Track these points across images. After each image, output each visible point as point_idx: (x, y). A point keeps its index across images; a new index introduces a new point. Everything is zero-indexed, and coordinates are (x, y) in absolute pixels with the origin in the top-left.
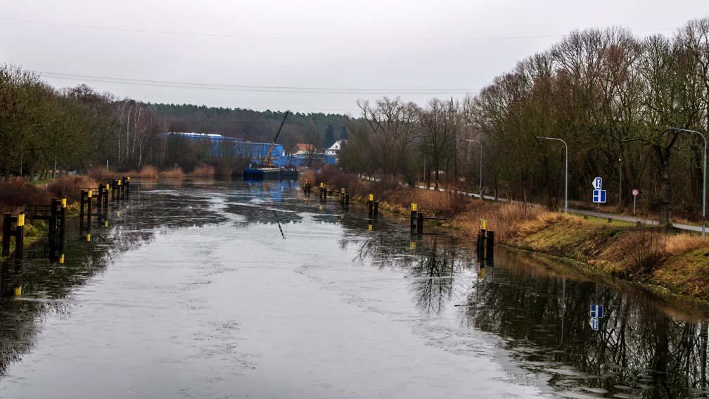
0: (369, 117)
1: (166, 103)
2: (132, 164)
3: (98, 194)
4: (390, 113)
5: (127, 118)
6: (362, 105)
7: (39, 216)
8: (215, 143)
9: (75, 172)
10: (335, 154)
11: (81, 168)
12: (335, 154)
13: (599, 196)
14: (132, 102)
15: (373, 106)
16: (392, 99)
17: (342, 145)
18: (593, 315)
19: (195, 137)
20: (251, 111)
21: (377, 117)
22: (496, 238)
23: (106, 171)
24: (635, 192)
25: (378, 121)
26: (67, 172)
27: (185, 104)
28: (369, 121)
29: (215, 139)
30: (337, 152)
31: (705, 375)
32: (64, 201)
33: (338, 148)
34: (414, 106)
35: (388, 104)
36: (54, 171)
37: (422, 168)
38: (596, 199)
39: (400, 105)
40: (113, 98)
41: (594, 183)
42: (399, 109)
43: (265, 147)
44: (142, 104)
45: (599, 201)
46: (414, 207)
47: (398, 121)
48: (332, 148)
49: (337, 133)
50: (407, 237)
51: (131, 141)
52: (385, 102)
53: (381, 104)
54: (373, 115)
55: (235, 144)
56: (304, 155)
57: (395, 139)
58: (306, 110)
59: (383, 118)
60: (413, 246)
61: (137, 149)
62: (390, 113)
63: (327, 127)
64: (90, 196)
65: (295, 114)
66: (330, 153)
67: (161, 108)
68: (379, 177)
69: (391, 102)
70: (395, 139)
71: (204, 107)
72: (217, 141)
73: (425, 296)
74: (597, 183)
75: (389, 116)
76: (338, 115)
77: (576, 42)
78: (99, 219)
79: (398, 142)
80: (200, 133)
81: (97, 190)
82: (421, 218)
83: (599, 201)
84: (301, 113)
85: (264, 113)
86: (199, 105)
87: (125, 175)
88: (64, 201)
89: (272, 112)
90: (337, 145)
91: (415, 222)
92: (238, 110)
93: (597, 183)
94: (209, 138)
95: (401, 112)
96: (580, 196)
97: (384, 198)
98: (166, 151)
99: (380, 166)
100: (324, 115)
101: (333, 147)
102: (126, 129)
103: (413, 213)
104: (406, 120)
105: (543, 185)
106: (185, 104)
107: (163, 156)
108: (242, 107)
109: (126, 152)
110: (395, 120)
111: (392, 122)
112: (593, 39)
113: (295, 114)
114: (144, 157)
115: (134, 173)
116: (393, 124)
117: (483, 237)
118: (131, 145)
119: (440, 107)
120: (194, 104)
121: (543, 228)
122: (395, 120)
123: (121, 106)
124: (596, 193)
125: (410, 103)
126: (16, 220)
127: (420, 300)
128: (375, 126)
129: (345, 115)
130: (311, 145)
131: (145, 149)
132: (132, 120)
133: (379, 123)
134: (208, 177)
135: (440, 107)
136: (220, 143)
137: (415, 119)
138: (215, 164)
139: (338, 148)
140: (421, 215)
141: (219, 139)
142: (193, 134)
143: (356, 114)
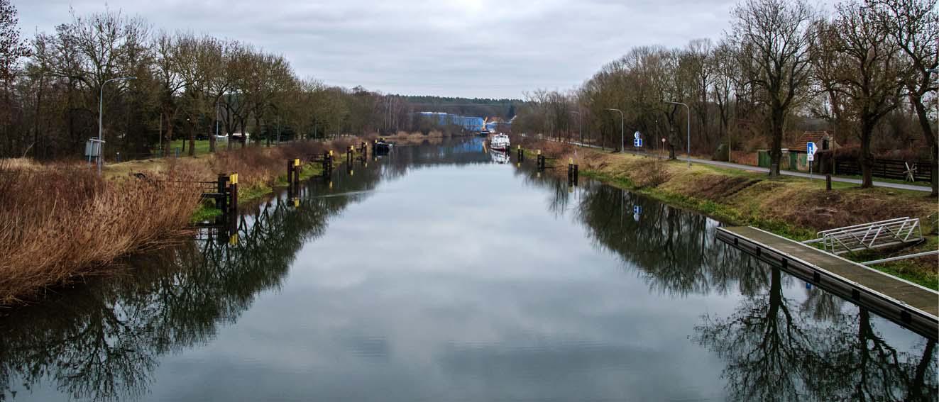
13: (638, 142)
16: (543, 89)
18: (636, 212)
19: (431, 115)
22: (579, 169)
24: (664, 140)
27: (476, 99)
29: (442, 115)
31: (190, 147)
38: (637, 144)
41: (635, 135)
42: (547, 95)
45: (638, 145)
51: (392, 117)
58: (498, 98)
61: (395, 122)
68: (540, 138)
73: (554, 204)
74: (637, 135)
77: (635, 52)
78: (362, 163)
82: (543, 159)
83: (638, 145)
84: (495, 99)
86: (436, 96)
91: (540, 161)
93: (637, 135)
94: (438, 115)
96: (629, 143)
105: (614, 138)
106: (476, 99)
107: (410, 126)
112: (645, 51)
114: (400, 126)
115: (394, 136)
117: (572, 169)
121: (622, 163)
124: (636, 141)
126: (294, 162)
127: (551, 207)
132: (392, 106)
138: (442, 130)
140: (543, 157)
141: (444, 115)
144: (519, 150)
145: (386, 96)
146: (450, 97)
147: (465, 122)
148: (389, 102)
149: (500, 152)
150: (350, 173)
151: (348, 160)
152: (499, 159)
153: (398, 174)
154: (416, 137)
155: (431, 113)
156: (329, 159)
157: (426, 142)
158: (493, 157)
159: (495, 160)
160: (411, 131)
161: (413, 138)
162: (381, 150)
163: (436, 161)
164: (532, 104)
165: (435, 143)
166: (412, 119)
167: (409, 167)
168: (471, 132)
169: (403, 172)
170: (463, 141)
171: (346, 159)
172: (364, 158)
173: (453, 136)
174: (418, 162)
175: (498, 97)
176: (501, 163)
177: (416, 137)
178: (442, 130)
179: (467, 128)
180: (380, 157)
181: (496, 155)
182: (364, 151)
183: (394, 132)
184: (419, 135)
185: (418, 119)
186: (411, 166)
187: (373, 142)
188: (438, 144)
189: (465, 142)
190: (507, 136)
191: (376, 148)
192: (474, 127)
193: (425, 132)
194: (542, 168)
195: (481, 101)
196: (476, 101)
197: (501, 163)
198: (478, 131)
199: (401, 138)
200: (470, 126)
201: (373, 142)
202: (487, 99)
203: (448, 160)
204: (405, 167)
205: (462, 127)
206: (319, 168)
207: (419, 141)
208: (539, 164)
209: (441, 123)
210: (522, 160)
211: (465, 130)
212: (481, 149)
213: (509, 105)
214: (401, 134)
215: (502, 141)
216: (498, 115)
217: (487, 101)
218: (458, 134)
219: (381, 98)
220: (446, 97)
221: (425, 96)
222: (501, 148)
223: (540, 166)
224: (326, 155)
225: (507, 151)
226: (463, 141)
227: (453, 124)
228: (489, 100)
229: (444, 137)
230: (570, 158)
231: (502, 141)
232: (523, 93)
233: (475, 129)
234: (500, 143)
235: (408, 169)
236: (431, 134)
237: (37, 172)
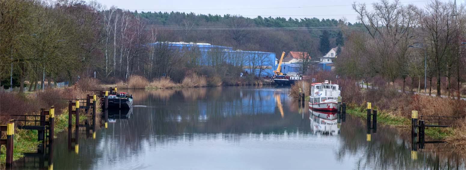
0: (366, 21)
1: (153, 12)
2: (342, 76)
3: (85, 104)
4: (388, 17)
5: (114, 27)
6: (358, 8)
7: (420, 129)
8: (204, 52)
9: (63, 83)
10: (330, 62)
11: (69, 80)
12: (330, 62)
14: (119, 11)
15: (370, 10)
17: (338, 52)
19: (185, 48)
20: (241, 18)
21: (375, 22)
23: (93, 83)
25: (376, 26)
26: (55, 84)
27: (259, 17)
28: (367, 27)
29: (204, 48)
30: (333, 59)
32: (52, 112)
33: (334, 56)
34: (414, 9)
35: (386, 7)
36: (42, 82)
37: (423, 74)
39: (399, 7)
40: (99, 7)
42: (399, 13)
43: (256, 56)
44: (128, 13)
46: (415, 114)
47: (397, 26)
48: (327, 56)
49: (332, 40)
50: (408, 145)
51: (118, 51)
52: (383, 5)
53: (378, 8)
54: (371, 20)
55: (225, 52)
56: (298, 63)
57: (394, 44)
59: (381, 23)
60: (414, 155)
61: (125, 60)
62: (388, 17)
63: (321, 34)
64: (78, 106)
65: (321, 20)
66: (325, 61)
67: (149, 17)
69: (390, 4)
70: (394, 44)
71: (192, 14)
72: (206, 50)
75: (388, 20)
76: (333, 20)
78: (88, 130)
79: (397, 47)
80: (189, 42)
81: (85, 101)
82: (422, 127)
84: (293, 18)
85: (255, 20)
86: (188, 12)
87: (112, 86)
88: (52, 112)
89: (263, 18)
90: (332, 53)
91: (417, 130)
92: (227, 17)
94: (198, 48)
95: (400, 15)
97: (384, 107)
98: (154, 62)
99: (377, 72)
100: (318, 20)
101: (329, 55)
102: (113, 38)
103: (414, 121)
104: (406, 25)
107: (150, 66)
108: (232, 14)
109: (113, 62)
110: (394, 25)
111: (391, 27)
113: (321, 20)
114: (131, 68)
115: (121, 84)
116: (395, 31)
118: (118, 56)
119: (441, 10)
120: (181, 12)
122: (394, 25)
123: (107, 16)
125: (410, 6)
128: (372, 30)
129: (340, 20)
130: (306, 53)
131: (132, 59)
132: (119, 31)
133: (377, 29)
134: (246, 85)
135: (441, 10)
136: (208, 52)
137: (416, 24)
138: (205, 73)
139: (334, 56)
142: (181, 43)
143: (352, 19)
144: (369, 111)
145: (108, 12)
146: (213, 14)
147: (247, 60)
148: (112, 21)
149: (325, 115)
150: (74, 149)
151: (70, 126)
152: (322, 128)
153: (129, 150)
154: (161, 87)
155: (184, 43)
156: (47, 123)
157: (178, 96)
158: (313, 124)
159: (315, 129)
160: (151, 77)
161: (157, 88)
162: (116, 108)
163: (192, 130)
164: (372, 30)
165: (195, 97)
166: (152, 55)
167: (148, 139)
168: (257, 78)
169: (136, 149)
170: (241, 94)
171: (67, 123)
172: (90, 123)
173: (226, 85)
174: (167, 130)
175: (298, 14)
176: (326, 134)
177: (161, 87)
178: (205, 73)
179: (249, 71)
180: (112, 121)
181: (316, 119)
182: (91, 110)
183: (122, 76)
184: (166, 82)
185: (163, 53)
186: (152, 139)
187: (101, 94)
188: (199, 98)
189: (245, 95)
190: (337, 86)
191: (107, 106)
192: (262, 69)
193: (177, 78)
194: (419, 142)
195: (268, 22)
196: (259, 21)
197: (326, 134)
198: (268, 77)
199: (135, 89)
200: (254, 69)
201: (101, 94)
202: (278, 19)
203: (211, 129)
204: (140, 138)
205: (239, 70)
206: (31, 139)
207: (167, 94)
208: (414, 135)
209: (204, 61)
210: (375, 128)
211: (246, 73)
212: (273, 109)
213: (317, 31)
214: (135, 80)
215: (328, 94)
216: (302, 47)
217: (279, 23)
218: (234, 82)
219: (100, 15)
220: (207, 14)
221: (169, 12)
222: (325, 107)
223: (417, 139)
224: (43, 117)
225: (339, 112)
226: (241, 94)
227: (224, 64)
228: (284, 20)
229: (210, 86)
230: (179, 121)
231: (328, 94)
232: (354, 7)
233: (264, 73)
234: (324, 99)
235: (145, 144)
236: (187, 80)
237: (439, 137)
